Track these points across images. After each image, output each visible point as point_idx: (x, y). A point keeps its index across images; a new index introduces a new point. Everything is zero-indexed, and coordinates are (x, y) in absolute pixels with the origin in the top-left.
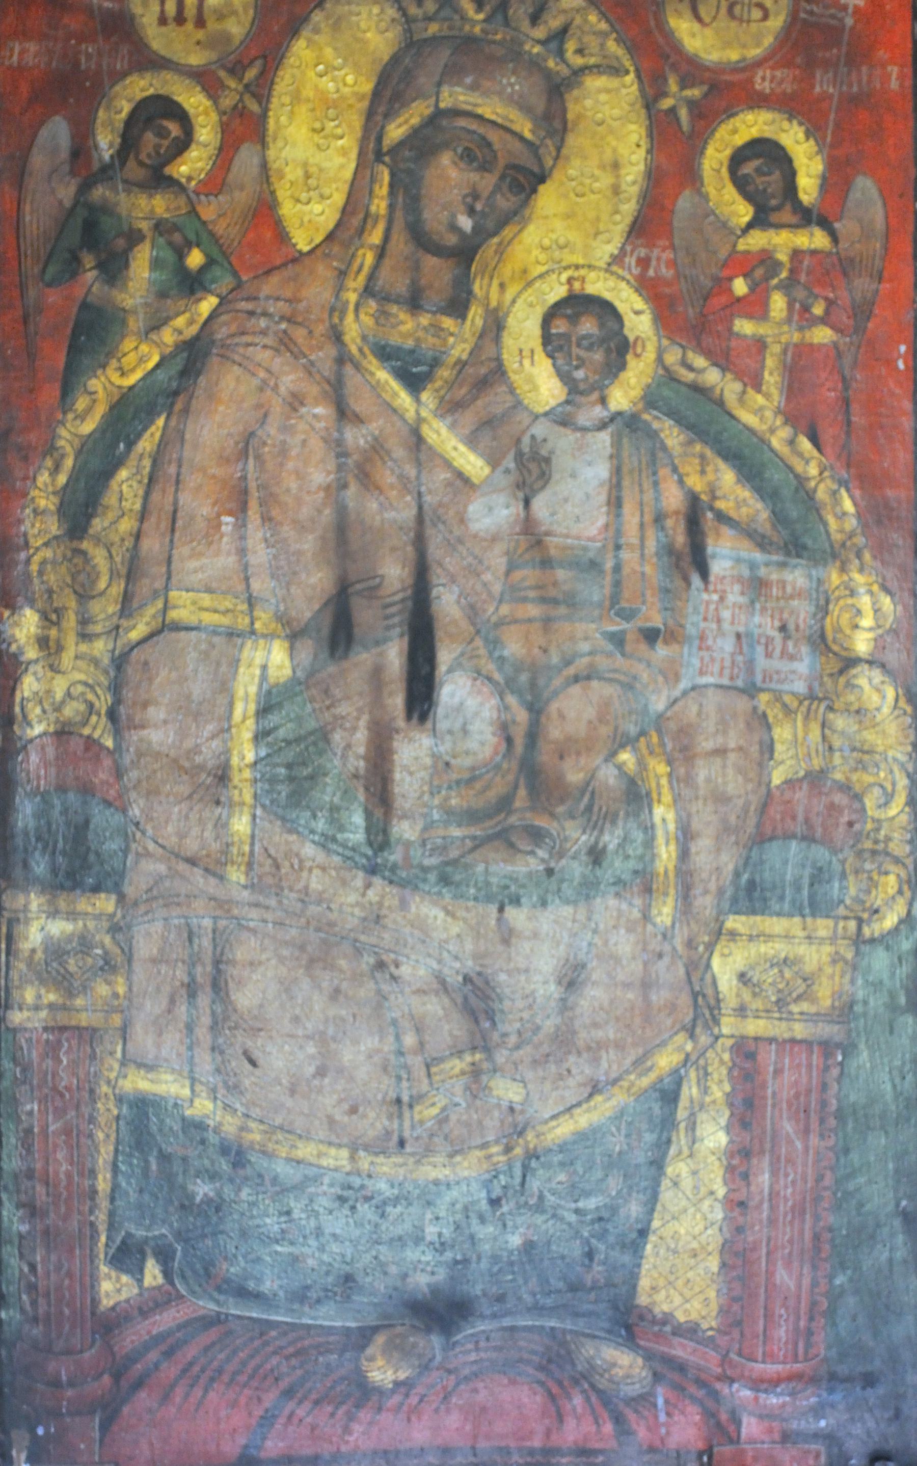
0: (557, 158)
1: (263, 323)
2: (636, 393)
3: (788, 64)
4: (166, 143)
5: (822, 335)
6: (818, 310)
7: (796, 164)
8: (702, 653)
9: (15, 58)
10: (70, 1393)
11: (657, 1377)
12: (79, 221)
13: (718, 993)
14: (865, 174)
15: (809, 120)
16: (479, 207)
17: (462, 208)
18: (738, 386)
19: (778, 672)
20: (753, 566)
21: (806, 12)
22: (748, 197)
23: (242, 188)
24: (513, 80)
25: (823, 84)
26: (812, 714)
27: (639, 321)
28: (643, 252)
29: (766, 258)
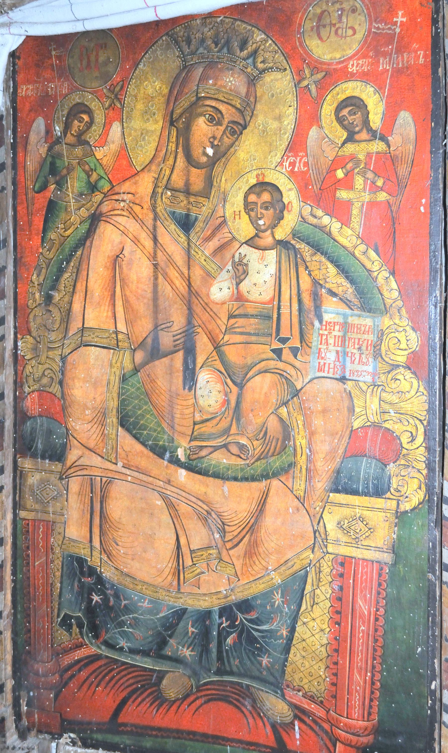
0: (251, 117)
1: (122, 204)
2: (288, 230)
3: (365, 56)
4: (82, 125)
5: (382, 196)
6: (380, 183)
7: (369, 108)
8: (320, 361)
9: (24, 93)
10: (43, 679)
11: (296, 717)
12: (48, 163)
13: (326, 531)
14: (405, 110)
15: (376, 85)
16: (216, 143)
17: (208, 144)
18: (338, 225)
19: (357, 371)
20: (345, 316)
21: (375, 27)
22: (344, 127)
23: (113, 142)
24: (231, 79)
25: (384, 65)
26: (374, 394)
27: (290, 195)
28: (292, 159)
29: (352, 158)
